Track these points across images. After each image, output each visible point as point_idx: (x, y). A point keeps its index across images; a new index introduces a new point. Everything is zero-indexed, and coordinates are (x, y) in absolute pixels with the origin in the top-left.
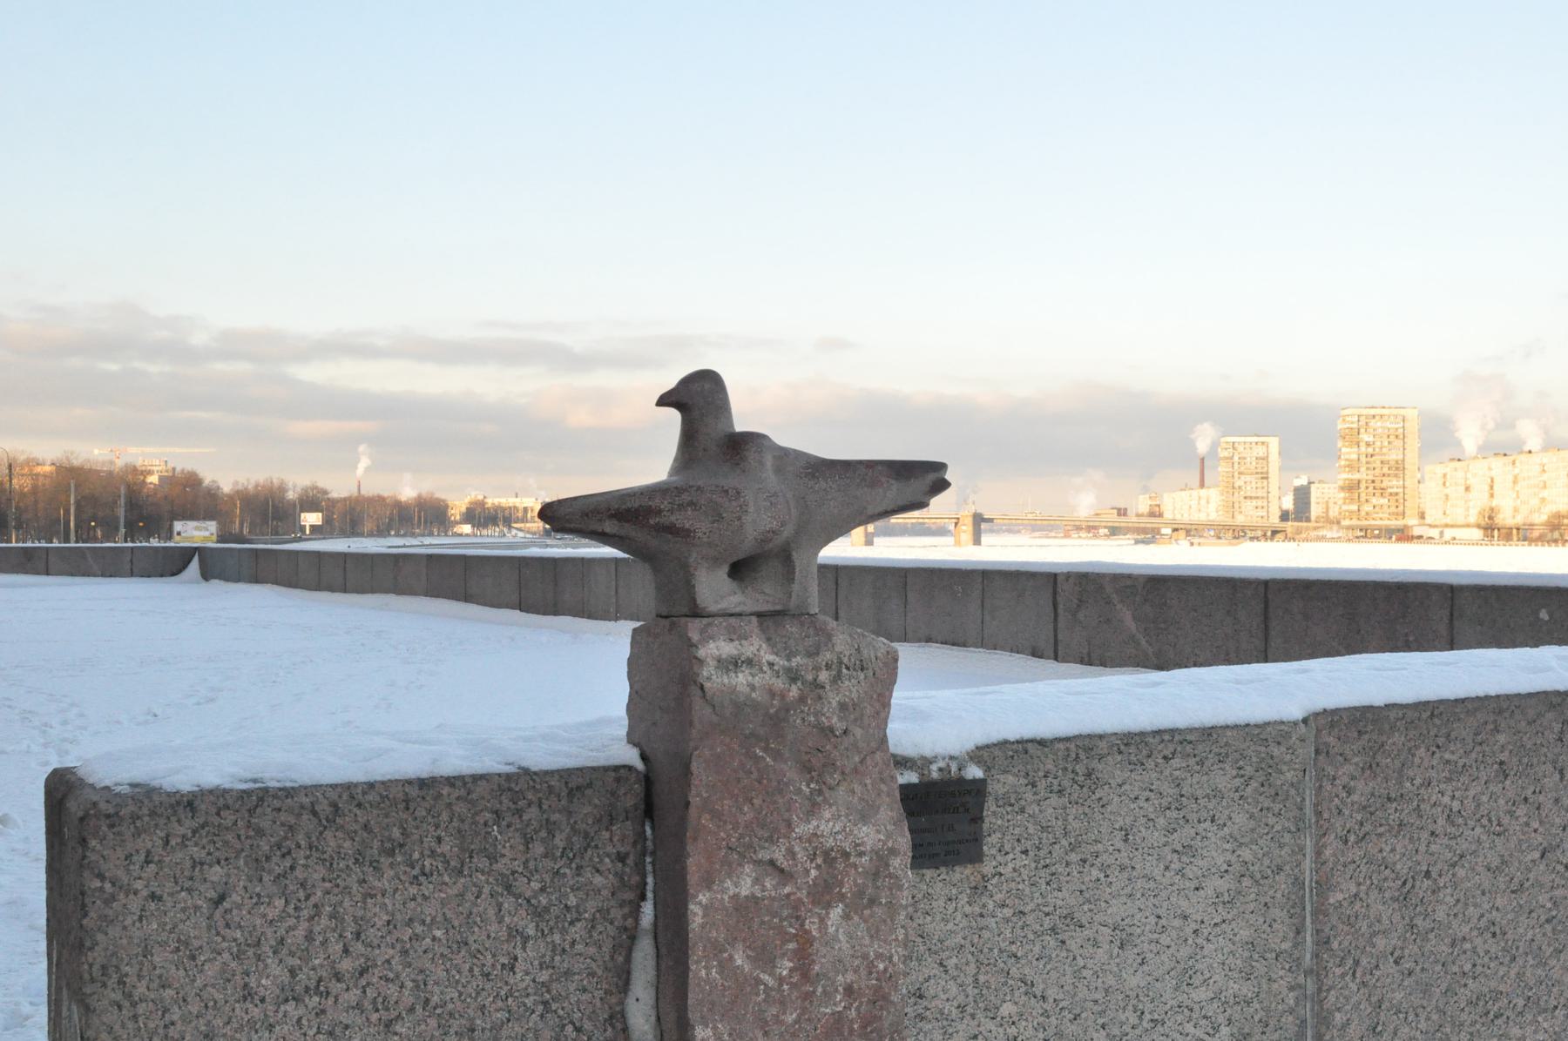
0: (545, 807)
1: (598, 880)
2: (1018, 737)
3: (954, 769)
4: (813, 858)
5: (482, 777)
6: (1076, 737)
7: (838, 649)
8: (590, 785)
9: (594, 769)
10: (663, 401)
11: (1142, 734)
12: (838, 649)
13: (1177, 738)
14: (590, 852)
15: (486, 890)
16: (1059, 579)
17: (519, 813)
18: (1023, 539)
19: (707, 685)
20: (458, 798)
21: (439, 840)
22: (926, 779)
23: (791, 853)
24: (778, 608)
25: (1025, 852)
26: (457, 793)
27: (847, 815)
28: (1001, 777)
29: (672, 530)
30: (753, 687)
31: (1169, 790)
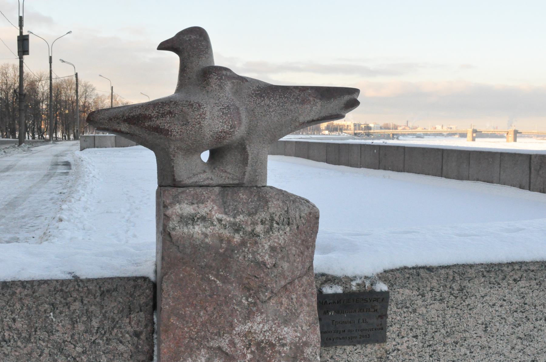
0: (85, 302)
1: (121, 347)
2: (414, 265)
3: (368, 284)
4: (248, 347)
5: (45, 282)
6: (455, 266)
7: (272, 210)
8: (115, 290)
9: (121, 278)
10: (164, 46)
11: (500, 265)
12: (272, 210)
13: (524, 268)
14: (115, 331)
15: (46, 351)
16: (533, 157)
17: (68, 305)
18: (534, 140)
19: (173, 233)
20: (26, 295)
21: (14, 320)
22: (348, 290)
23: (232, 343)
24: (236, 182)
25: (416, 337)
26: (26, 292)
27: (273, 320)
28: (401, 291)
29: (157, 130)
30: (206, 236)
31: (515, 299)
